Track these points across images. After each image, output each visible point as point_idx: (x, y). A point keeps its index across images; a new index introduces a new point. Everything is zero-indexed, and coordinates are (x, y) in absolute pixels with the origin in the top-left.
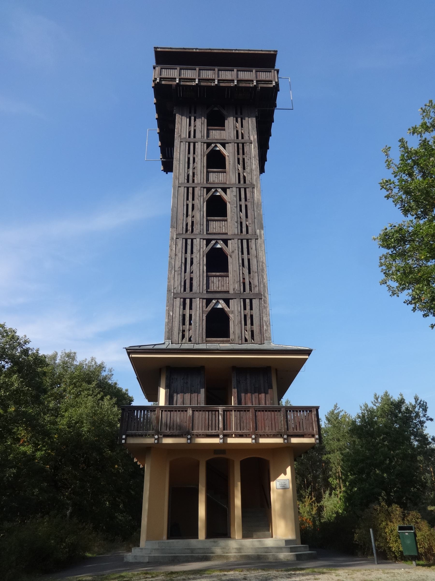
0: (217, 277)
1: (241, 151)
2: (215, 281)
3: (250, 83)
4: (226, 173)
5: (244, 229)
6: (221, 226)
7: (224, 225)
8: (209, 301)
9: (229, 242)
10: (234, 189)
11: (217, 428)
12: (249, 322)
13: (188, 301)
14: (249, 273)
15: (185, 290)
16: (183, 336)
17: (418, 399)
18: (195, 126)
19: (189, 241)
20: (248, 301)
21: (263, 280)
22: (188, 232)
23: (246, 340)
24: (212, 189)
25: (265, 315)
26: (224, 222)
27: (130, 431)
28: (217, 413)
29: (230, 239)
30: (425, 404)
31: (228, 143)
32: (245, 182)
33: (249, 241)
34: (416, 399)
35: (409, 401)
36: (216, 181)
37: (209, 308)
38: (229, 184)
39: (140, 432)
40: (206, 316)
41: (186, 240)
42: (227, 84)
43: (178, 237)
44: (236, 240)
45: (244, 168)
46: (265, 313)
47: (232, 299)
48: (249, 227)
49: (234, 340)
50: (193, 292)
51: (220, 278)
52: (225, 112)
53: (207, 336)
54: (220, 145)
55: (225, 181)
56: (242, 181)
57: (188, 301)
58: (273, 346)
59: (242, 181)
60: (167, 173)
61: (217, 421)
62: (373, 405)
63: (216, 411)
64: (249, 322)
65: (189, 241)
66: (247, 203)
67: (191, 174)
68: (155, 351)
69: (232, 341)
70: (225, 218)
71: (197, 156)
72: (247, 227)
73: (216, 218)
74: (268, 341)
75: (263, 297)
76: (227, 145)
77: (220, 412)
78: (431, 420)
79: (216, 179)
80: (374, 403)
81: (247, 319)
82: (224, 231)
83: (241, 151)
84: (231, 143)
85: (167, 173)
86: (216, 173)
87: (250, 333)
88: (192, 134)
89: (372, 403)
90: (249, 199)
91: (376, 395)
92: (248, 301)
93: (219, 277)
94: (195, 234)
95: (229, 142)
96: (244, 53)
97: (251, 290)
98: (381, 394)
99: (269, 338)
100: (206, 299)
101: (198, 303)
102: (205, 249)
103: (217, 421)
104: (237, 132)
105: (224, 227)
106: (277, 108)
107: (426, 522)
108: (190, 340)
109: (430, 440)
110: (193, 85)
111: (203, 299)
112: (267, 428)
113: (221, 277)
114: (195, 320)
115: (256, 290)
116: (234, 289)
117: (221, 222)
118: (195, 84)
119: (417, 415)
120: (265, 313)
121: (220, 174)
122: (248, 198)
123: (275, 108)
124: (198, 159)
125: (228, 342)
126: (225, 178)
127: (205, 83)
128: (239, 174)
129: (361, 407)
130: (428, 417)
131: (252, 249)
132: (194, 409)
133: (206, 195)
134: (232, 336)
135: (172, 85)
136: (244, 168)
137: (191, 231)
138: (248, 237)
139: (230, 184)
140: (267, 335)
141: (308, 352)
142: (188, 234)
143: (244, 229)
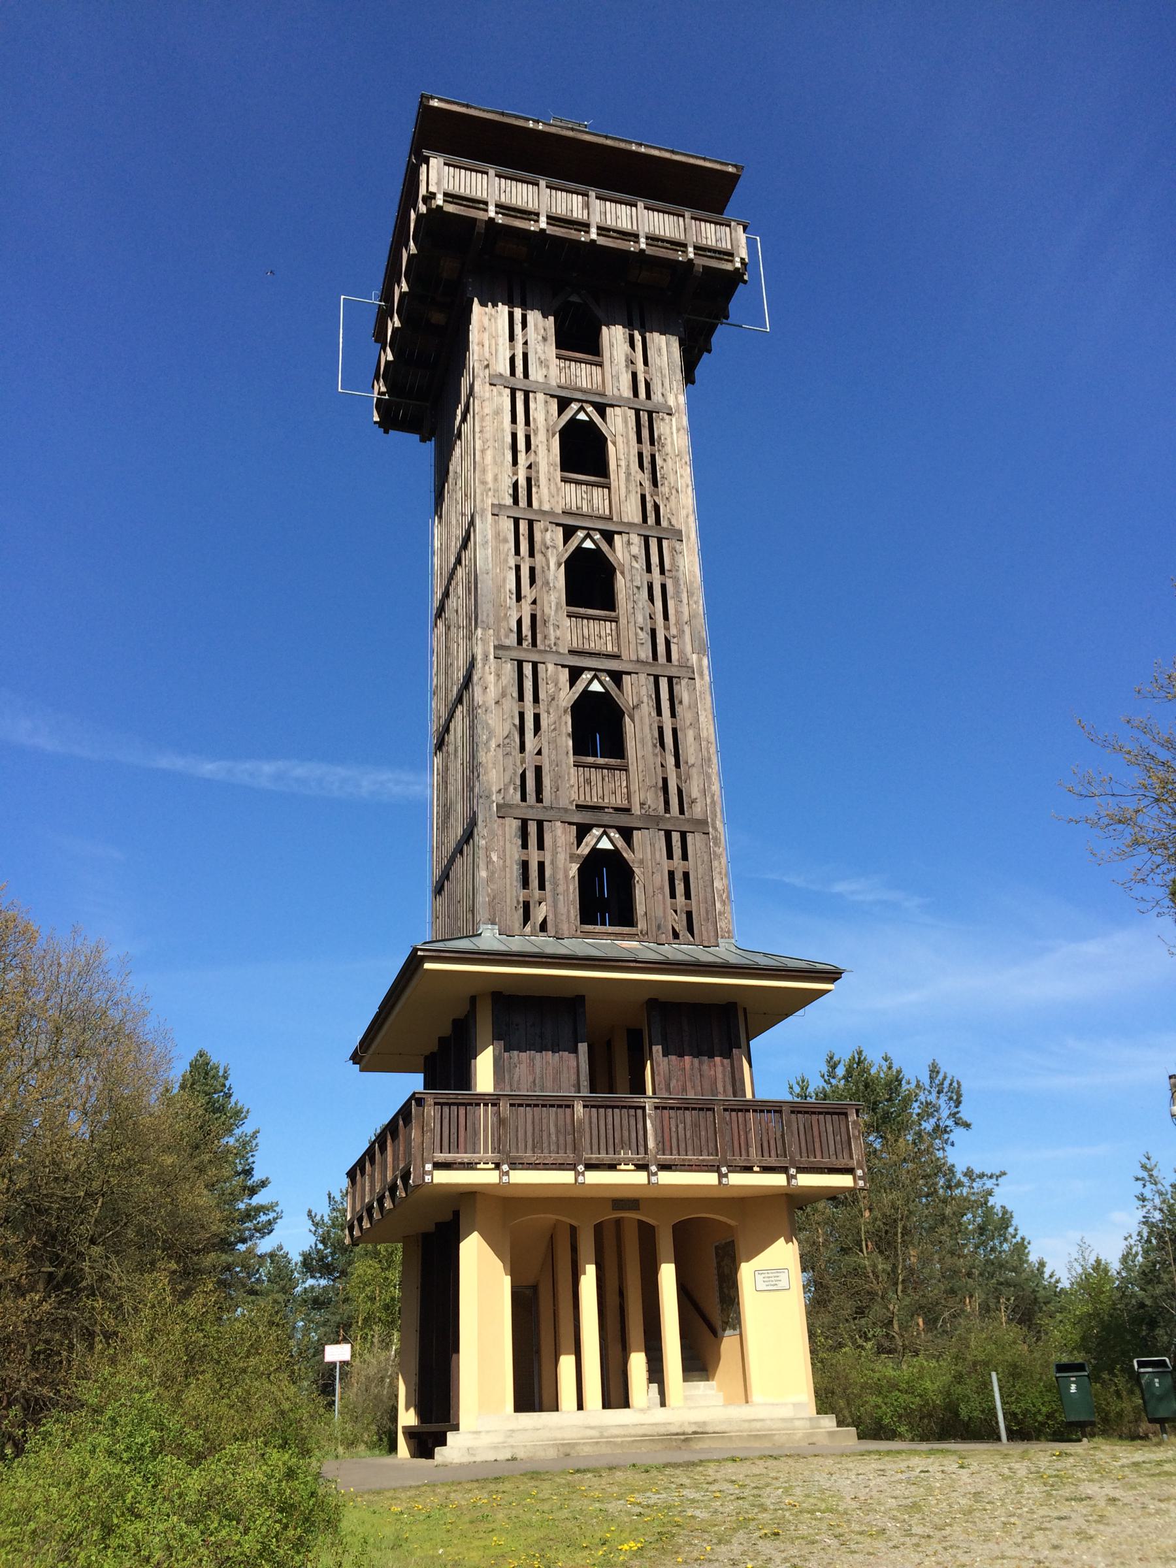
0: (611, 769)
1: (645, 433)
2: (593, 778)
3: (678, 251)
4: (609, 488)
5: (661, 648)
6: (603, 634)
7: (608, 631)
8: (583, 831)
9: (626, 679)
10: (636, 539)
11: (642, 1149)
12: (680, 888)
13: (532, 828)
14: (678, 765)
15: (524, 799)
16: (526, 918)
17: (938, 1072)
18: (526, 343)
19: (528, 669)
20: (676, 837)
21: (709, 787)
22: (525, 644)
23: (676, 935)
24: (576, 531)
25: (718, 876)
26: (608, 623)
27: (466, 1153)
28: (640, 1112)
29: (629, 673)
30: (955, 1084)
31: (612, 406)
32: (658, 521)
33: (675, 681)
34: (934, 1071)
35: (914, 1072)
36: (585, 509)
37: (585, 850)
38: (617, 523)
39: (465, 1157)
40: (579, 869)
41: (520, 664)
42: (619, 241)
43: (500, 653)
44: (643, 677)
45: (655, 483)
46: (718, 870)
47: (639, 829)
48: (672, 645)
49: (647, 933)
50: (545, 804)
51: (605, 771)
52: (600, 314)
53: (584, 921)
54: (591, 408)
55: (607, 512)
56: (651, 520)
57: (532, 828)
58: (725, 951)
59: (651, 520)
60: (386, 432)
61: (641, 1133)
62: (825, 1081)
63: (636, 1108)
64: (680, 888)
65: (528, 669)
66: (666, 865)
67: (522, 482)
68: (486, 957)
69: (643, 935)
70: (613, 614)
71: (536, 434)
72: (668, 643)
73: (590, 612)
74: (727, 940)
75: (711, 829)
76: (609, 410)
77: (647, 1111)
78: (967, 1126)
79: (585, 502)
80: (826, 1078)
81: (677, 882)
82: (610, 648)
83: (645, 433)
84: (620, 406)
85: (386, 432)
86: (584, 487)
87: (684, 916)
88: (520, 364)
89: (823, 1076)
90: (670, 571)
91: (831, 1058)
92: (676, 837)
93: (602, 768)
94: (541, 652)
95: (614, 403)
96: (659, 158)
97: (682, 812)
98: (844, 1055)
99: (729, 932)
100: (579, 826)
101: (560, 836)
102: (567, 696)
103: (641, 1133)
104: (634, 375)
105: (609, 638)
106: (729, 321)
107: (437, 1449)
108: (543, 927)
109: (959, 1175)
110: (530, 231)
111: (570, 823)
112: (753, 1151)
113: (608, 769)
114: (553, 876)
115: (697, 811)
116: (642, 804)
117: (602, 622)
118: (538, 230)
119: (929, 1110)
120: (718, 870)
121: (595, 489)
122: (667, 566)
123: (725, 321)
124: (539, 440)
125: (631, 937)
126: (607, 502)
127: (563, 230)
128: (643, 497)
129: (791, 1088)
130: (960, 1118)
131: (681, 702)
132: (588, 1103)
133: (564, 545)
134: (641, 925)
135: (474, 220)
136: (655, 483)
137: (530, 641)
138: (673, 672)
139: (622, 523)
140: (724, 926)
141: (833, 975)
142: (525, 650)
143: (661, 648)
